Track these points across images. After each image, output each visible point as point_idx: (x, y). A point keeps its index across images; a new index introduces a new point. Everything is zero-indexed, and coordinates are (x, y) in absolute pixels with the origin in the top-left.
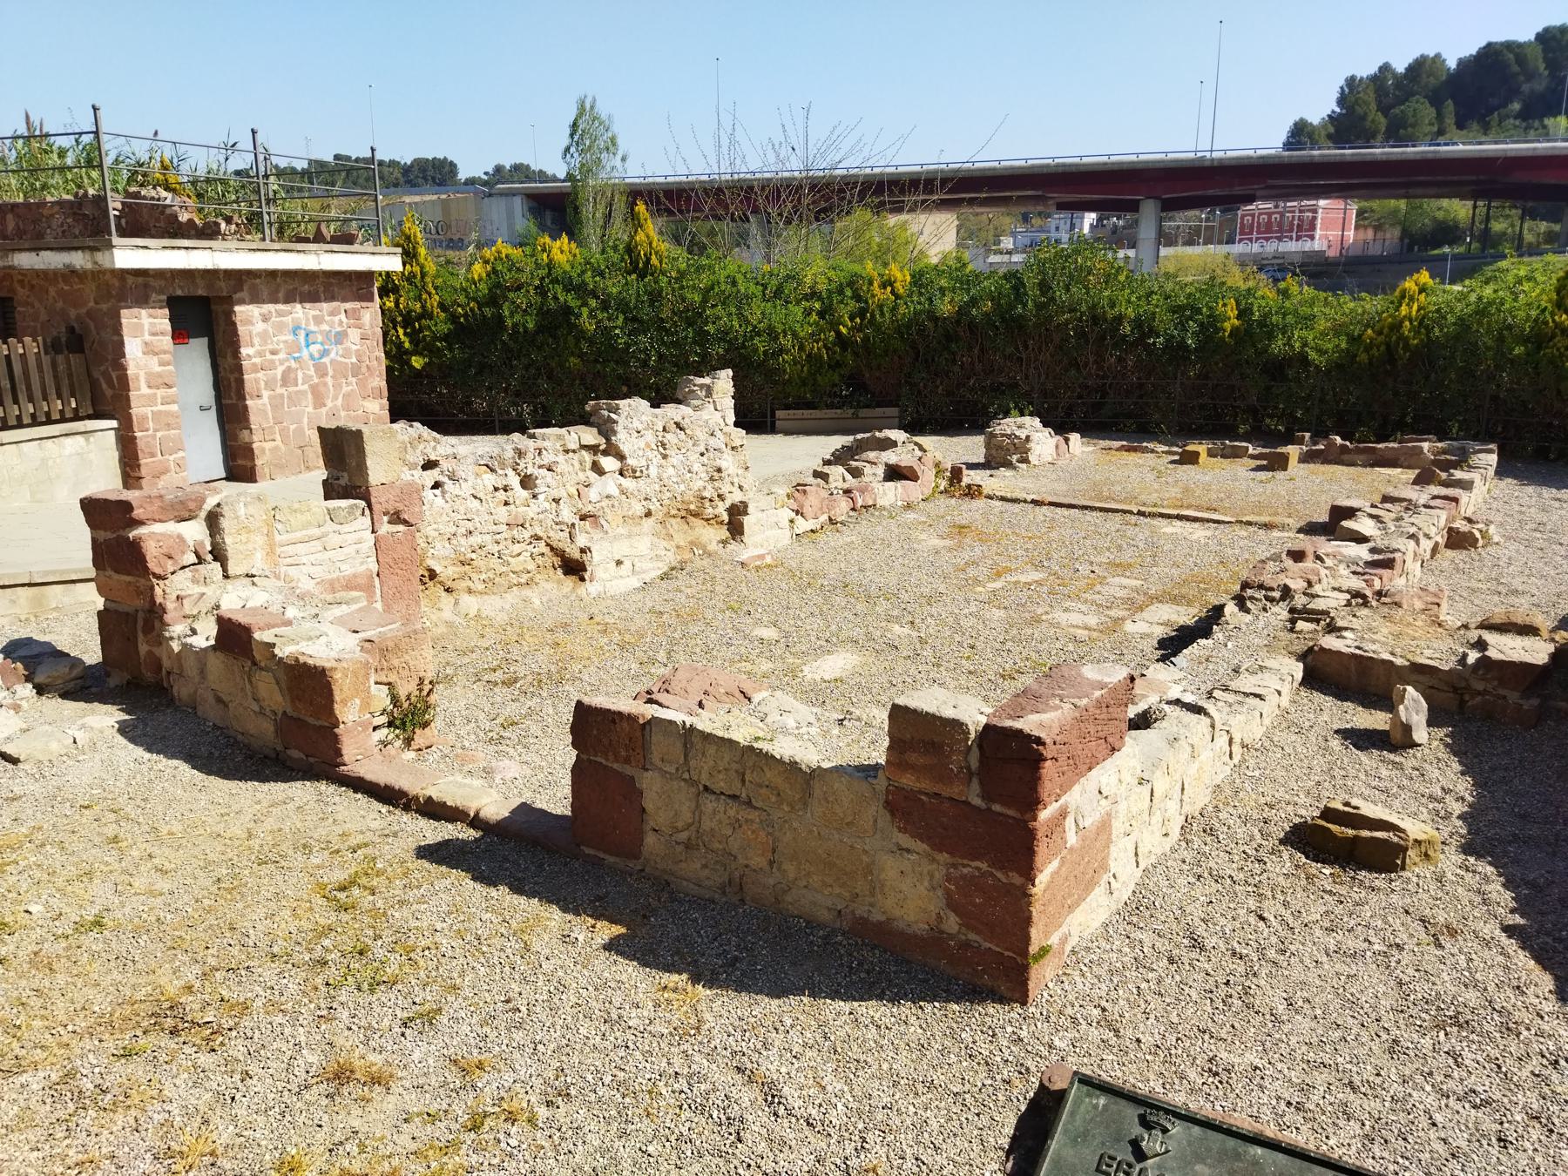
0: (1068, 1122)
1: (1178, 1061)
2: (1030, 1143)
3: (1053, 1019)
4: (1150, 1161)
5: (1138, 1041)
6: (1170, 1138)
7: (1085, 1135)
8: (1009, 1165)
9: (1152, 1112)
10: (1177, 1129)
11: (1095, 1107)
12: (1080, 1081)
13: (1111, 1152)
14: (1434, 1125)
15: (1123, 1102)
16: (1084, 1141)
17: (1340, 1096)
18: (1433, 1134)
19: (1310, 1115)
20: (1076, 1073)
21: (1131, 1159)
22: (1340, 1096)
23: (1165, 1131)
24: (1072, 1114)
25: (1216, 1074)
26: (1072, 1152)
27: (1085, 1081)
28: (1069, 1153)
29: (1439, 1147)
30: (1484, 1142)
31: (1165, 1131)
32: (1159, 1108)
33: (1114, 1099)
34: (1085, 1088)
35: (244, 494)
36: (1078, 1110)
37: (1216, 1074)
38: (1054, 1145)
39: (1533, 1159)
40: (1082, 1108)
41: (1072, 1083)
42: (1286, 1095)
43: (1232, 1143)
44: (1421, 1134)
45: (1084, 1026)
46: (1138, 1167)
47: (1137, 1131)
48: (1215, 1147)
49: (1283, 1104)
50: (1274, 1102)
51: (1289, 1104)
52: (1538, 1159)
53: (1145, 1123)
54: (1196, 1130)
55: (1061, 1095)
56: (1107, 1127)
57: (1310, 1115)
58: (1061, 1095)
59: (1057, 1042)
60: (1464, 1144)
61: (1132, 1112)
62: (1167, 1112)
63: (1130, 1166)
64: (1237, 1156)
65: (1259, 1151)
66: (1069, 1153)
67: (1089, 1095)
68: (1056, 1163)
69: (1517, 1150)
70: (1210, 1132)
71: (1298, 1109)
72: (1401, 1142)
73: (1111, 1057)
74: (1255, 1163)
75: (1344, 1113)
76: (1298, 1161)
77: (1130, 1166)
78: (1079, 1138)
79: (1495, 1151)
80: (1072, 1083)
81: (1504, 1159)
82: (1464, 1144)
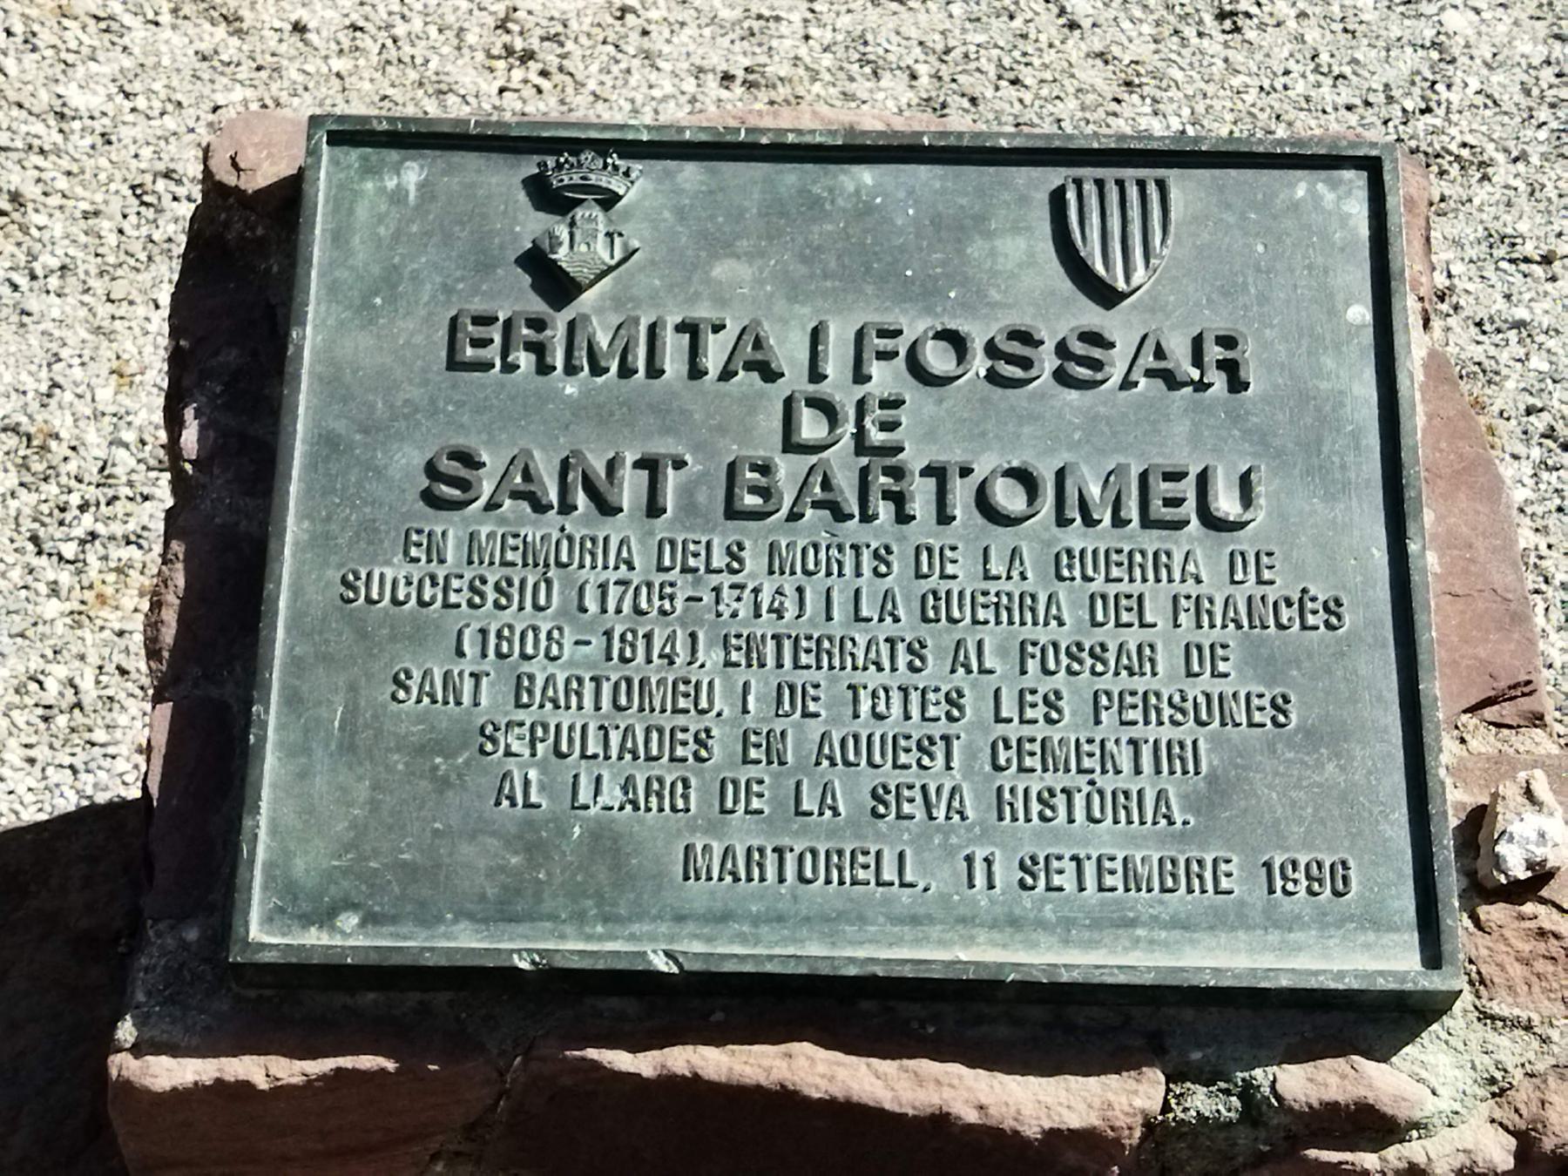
0: (329, 267)
1: (419, 52)
2: (231, 356)
3: (45, 37)
4: (588, 297)
5: (299, 28)
6: (627, 215)
7: (390, 281)
8: (190, 438)
9: (558, 165)
10: (638, 185)
11: (398, 197)
12: (336, 139)
13: (478, 306)
14: (1073, 26)
15: (471, 161)
16: (392, 300)
17: (844, 21)
18: (1075, 48)
19: (783, 91)
20: (314, 121)
21: (538, 306)
22: (844, 21)
23: (609, 200)
24: (338, 237)
25: (528, 56)
26: (365, 340)
27: (349, 135)
28: (360, 346)
29: (1096, 76)
30: (1189, 32)
31: (609, 200)
32: (575, 146)
33: (443, 159)
34: (354, 155)
35: (1400, 875)
36: (354, 222)
37: (528, 56)
38: (313, 337)
39: (1300, 39)
40: (362, 212)
41: (313, 152)
42: (717, 61)
43: (790, 176)
44: (1050, 56)
45: (138, 34)
46: (561, 320)
47: (532, 224)
48: (752, 203)
49: (712, 82)
50: (690, 85)
51: (727, 78)
52: (1312, 35)
53: (546, 197)
54: (690, 173)
55: (287, 201)
56: (448, 239)
57: (783, 91)
58: (287, 201)
59: (78, 99)
60: (1144, 50)
61: (503, 180)
62: (602, 147)
63: (538, 324)
64: (814, 206)
65: (866, 175)
66: (360, 346)
67: (369, 170)
68: (333, 384)
69: (1262, 27)
70: (728, 168)
71: (750, 85)
72: (1008, 91)
73: (238, 93)
74: (864, 210)
75: (863, 61)
76: (970, 171)
77: (538, 324)
78: (376, 295)
79: (1214, 46)
80: (313, 152)
81: (1238, 58)
82: (1144, 50)
